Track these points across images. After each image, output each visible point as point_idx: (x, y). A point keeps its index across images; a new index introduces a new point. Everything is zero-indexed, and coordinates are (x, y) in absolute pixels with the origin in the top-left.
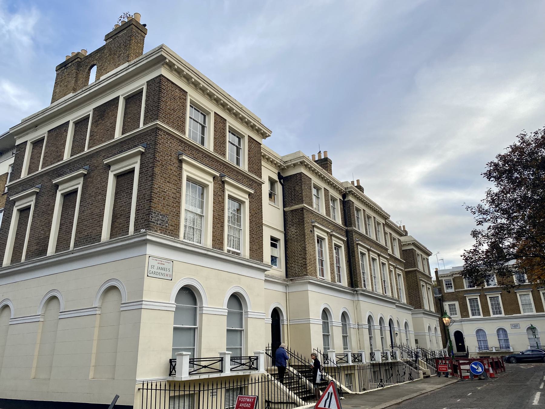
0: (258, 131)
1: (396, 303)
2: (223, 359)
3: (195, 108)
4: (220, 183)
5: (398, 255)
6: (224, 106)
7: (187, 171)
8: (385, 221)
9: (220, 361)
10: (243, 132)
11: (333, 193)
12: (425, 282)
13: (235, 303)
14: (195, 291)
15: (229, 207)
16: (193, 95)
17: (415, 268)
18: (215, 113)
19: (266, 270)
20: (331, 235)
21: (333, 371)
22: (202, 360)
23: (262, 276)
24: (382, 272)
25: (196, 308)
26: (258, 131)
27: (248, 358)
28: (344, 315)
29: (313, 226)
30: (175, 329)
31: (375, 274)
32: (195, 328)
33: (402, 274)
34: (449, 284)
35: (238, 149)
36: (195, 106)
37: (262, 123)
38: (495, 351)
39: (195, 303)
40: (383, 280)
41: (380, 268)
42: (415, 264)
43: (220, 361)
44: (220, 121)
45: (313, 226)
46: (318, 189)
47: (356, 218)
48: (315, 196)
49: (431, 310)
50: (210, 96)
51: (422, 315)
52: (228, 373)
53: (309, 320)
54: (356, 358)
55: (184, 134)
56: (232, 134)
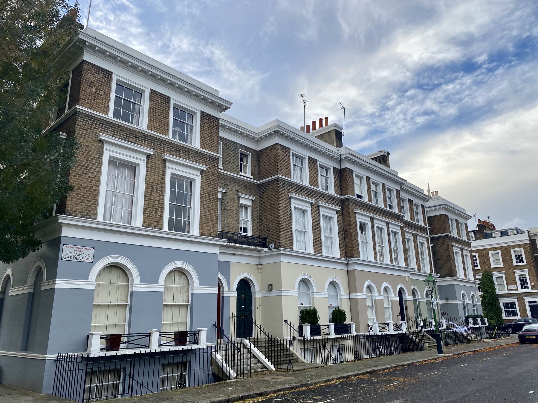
1: (411, 271)
2: (200, 332)
4: (316, 208)
6: (163, 81)
7: (294, 204)
8: (401, 187)
9: (328, 327)
10: (328, 165)
11: (322, 161)
16: (294, 149)
18: (308, 156)
20: (416, 235)
21: (331, 341)
22: (131, 335)
25: (128, 285)
27: (173, 333)
29: (290, 198)
32: (127, 304)
33: (335, 217)
34: (519, 256)
35: (326, 179)
36: (296, 156)
38: (379, 333)
43: (328, 327)
44: (313, 162)
45: (290, 197)
50: (144, 72)
52: (154, 348)
53: (280, 291)
55: (318, 187)
56: (322, 168)
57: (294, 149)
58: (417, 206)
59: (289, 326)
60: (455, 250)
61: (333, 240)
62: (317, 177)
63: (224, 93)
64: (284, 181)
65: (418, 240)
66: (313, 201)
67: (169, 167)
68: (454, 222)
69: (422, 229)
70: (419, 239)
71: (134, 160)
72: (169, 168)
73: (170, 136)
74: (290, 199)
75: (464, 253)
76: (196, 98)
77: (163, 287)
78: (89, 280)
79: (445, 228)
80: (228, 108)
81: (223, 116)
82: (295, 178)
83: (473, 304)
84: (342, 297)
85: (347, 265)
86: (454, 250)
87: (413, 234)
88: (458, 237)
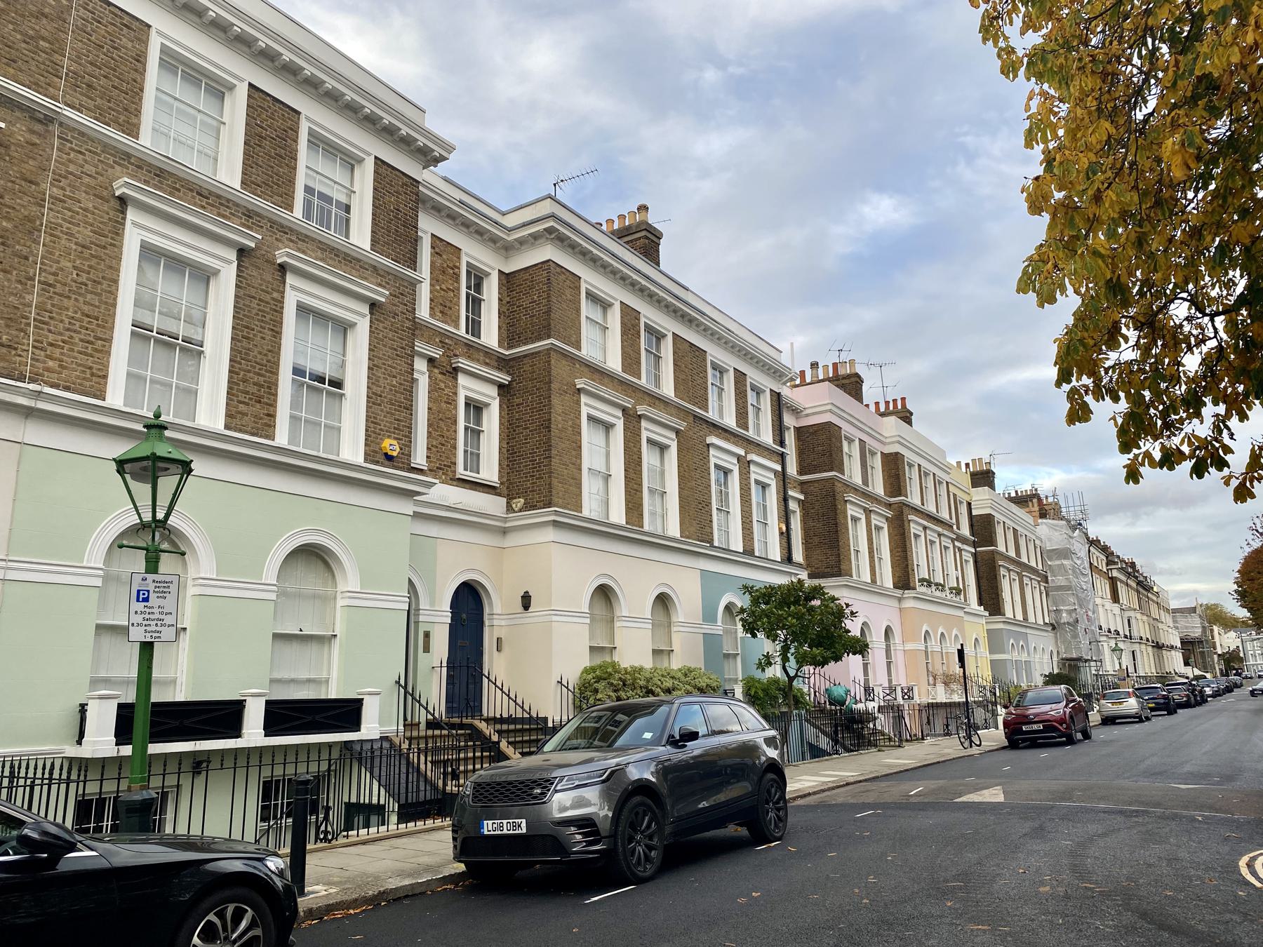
0: (405, 144)
3: (343, 157)
4: (632, 420)
5: (965, 531)
6: (289, 72)
7: (587, 406)
12: (1008, 569)
13: (660, 609)
14: (326, 553)
15: (649, 458)
16: (590, 279)
17: (549, 337)
19: (419, 493)
23: (408, 508)
24: (944, 560)
26: (405, 144)
28: (888, 632)
30: (591, 648)
31: (918, 561)
33: (886, 527)
36: (593, 297)
37: (782, 362)
39: (668, 615)
40: (945, 573)
41: (927, 547)
42: (991, 541)
46: (721, 371)
47: (908, 480)
48: (754, 406)
49: (1017, 618)
51: (550, 534)
54: (906, 694)
55: (640, 378)
57: (590, 279)
58: (758, 392)
59: (565, 690)
60: (851, 511)
61: (668, 497)
62: (706, 389)
63: (438, 125)
64: (565, 355)
65: (753, 477)
66: (742, 452)
67: (134, 224)
68: (766, 403)
69: (964, 540)
70: (755, 473)
71: (608, 416)
72: (293, 288)
73: (298, 211)
74: (579, 394)
75: (874, 522)
76: (351, 114)
77: (588, 615)
78: (85, 564)
79: (833, 459)
80: (444, 159)
81: (429, 177)
82: (588, 351)
83: (926, 652)
84: (898, 648)
85: (900, 600)
86: (850, 513)
87: (739, 458)
88: (676, 399)
